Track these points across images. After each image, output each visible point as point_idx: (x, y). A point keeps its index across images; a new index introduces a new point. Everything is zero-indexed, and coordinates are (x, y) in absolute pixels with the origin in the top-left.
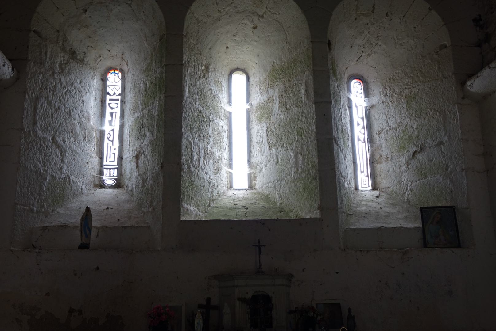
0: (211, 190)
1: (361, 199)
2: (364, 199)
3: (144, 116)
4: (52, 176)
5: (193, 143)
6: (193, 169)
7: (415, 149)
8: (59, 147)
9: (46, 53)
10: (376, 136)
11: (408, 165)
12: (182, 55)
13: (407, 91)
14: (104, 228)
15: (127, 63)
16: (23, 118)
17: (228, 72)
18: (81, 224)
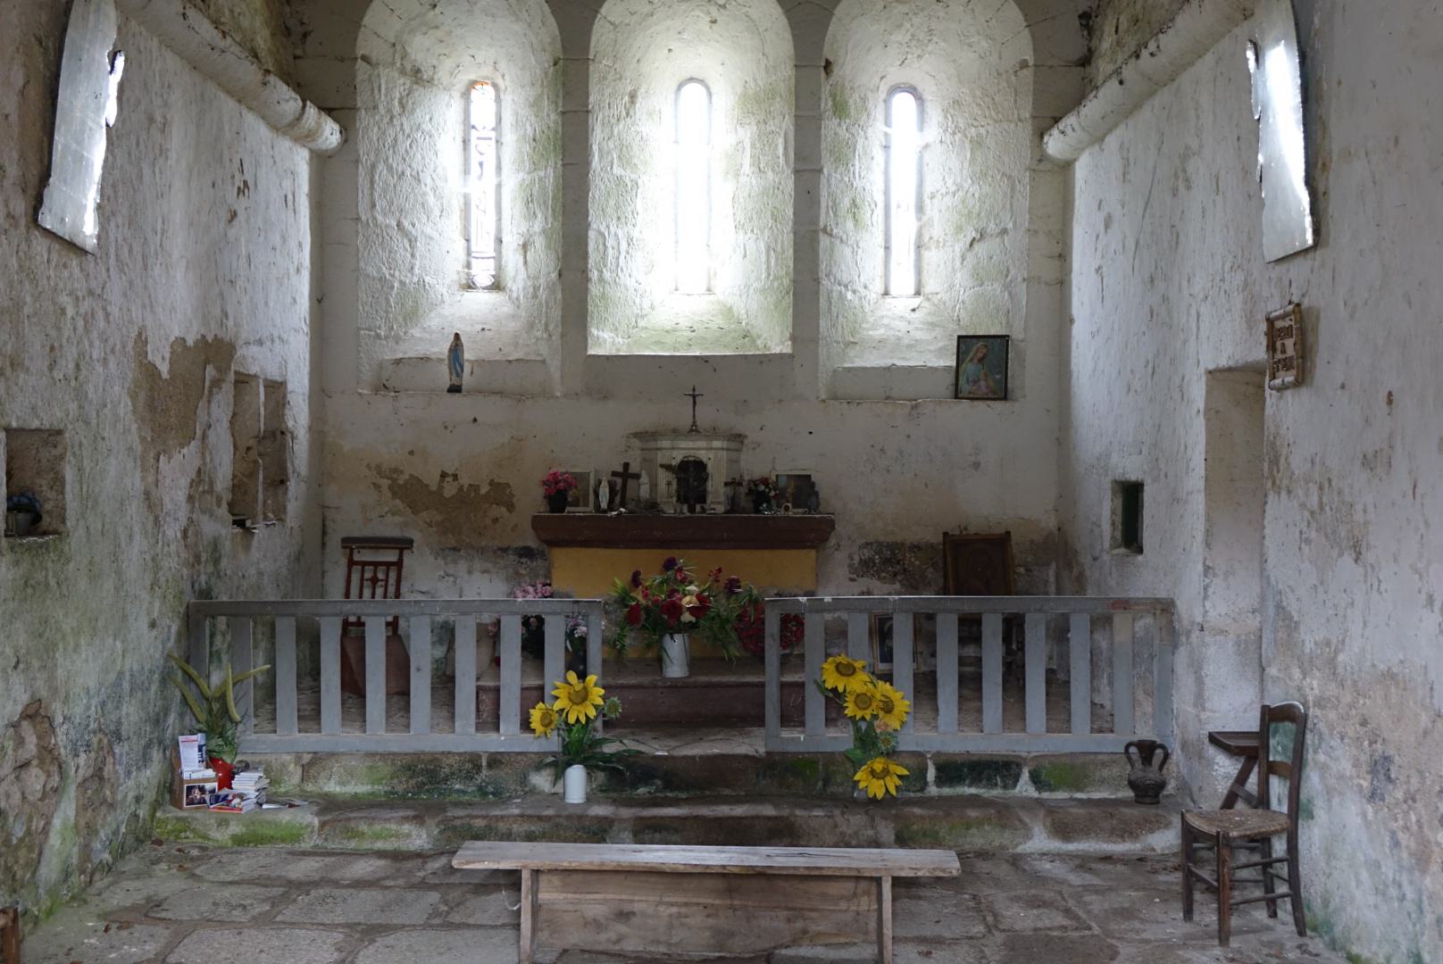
0: (638, 301)
1: (885, 313)
2: (889, 314)
3: (533, 182)
4: (401, 282)
5: (606, 234)
6: (607, 275)
7: (974, 234)
8: (407, 235)
9: (380, 87)
10: (927, 201)
11: (963, 260)
12: (587, 95)
13: (973, 129)
14: (479, 363)
15: (503, 76)
16: (357, 202)
17: (675, 87)
18: (449, 357)
